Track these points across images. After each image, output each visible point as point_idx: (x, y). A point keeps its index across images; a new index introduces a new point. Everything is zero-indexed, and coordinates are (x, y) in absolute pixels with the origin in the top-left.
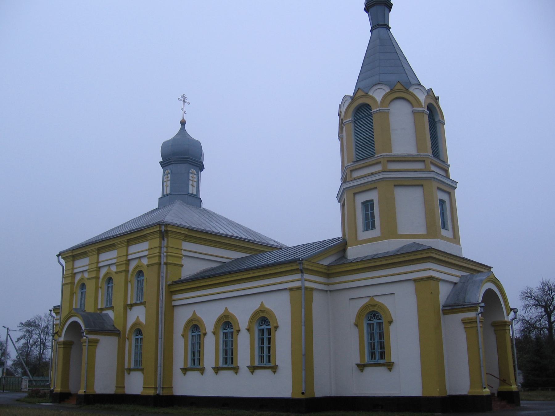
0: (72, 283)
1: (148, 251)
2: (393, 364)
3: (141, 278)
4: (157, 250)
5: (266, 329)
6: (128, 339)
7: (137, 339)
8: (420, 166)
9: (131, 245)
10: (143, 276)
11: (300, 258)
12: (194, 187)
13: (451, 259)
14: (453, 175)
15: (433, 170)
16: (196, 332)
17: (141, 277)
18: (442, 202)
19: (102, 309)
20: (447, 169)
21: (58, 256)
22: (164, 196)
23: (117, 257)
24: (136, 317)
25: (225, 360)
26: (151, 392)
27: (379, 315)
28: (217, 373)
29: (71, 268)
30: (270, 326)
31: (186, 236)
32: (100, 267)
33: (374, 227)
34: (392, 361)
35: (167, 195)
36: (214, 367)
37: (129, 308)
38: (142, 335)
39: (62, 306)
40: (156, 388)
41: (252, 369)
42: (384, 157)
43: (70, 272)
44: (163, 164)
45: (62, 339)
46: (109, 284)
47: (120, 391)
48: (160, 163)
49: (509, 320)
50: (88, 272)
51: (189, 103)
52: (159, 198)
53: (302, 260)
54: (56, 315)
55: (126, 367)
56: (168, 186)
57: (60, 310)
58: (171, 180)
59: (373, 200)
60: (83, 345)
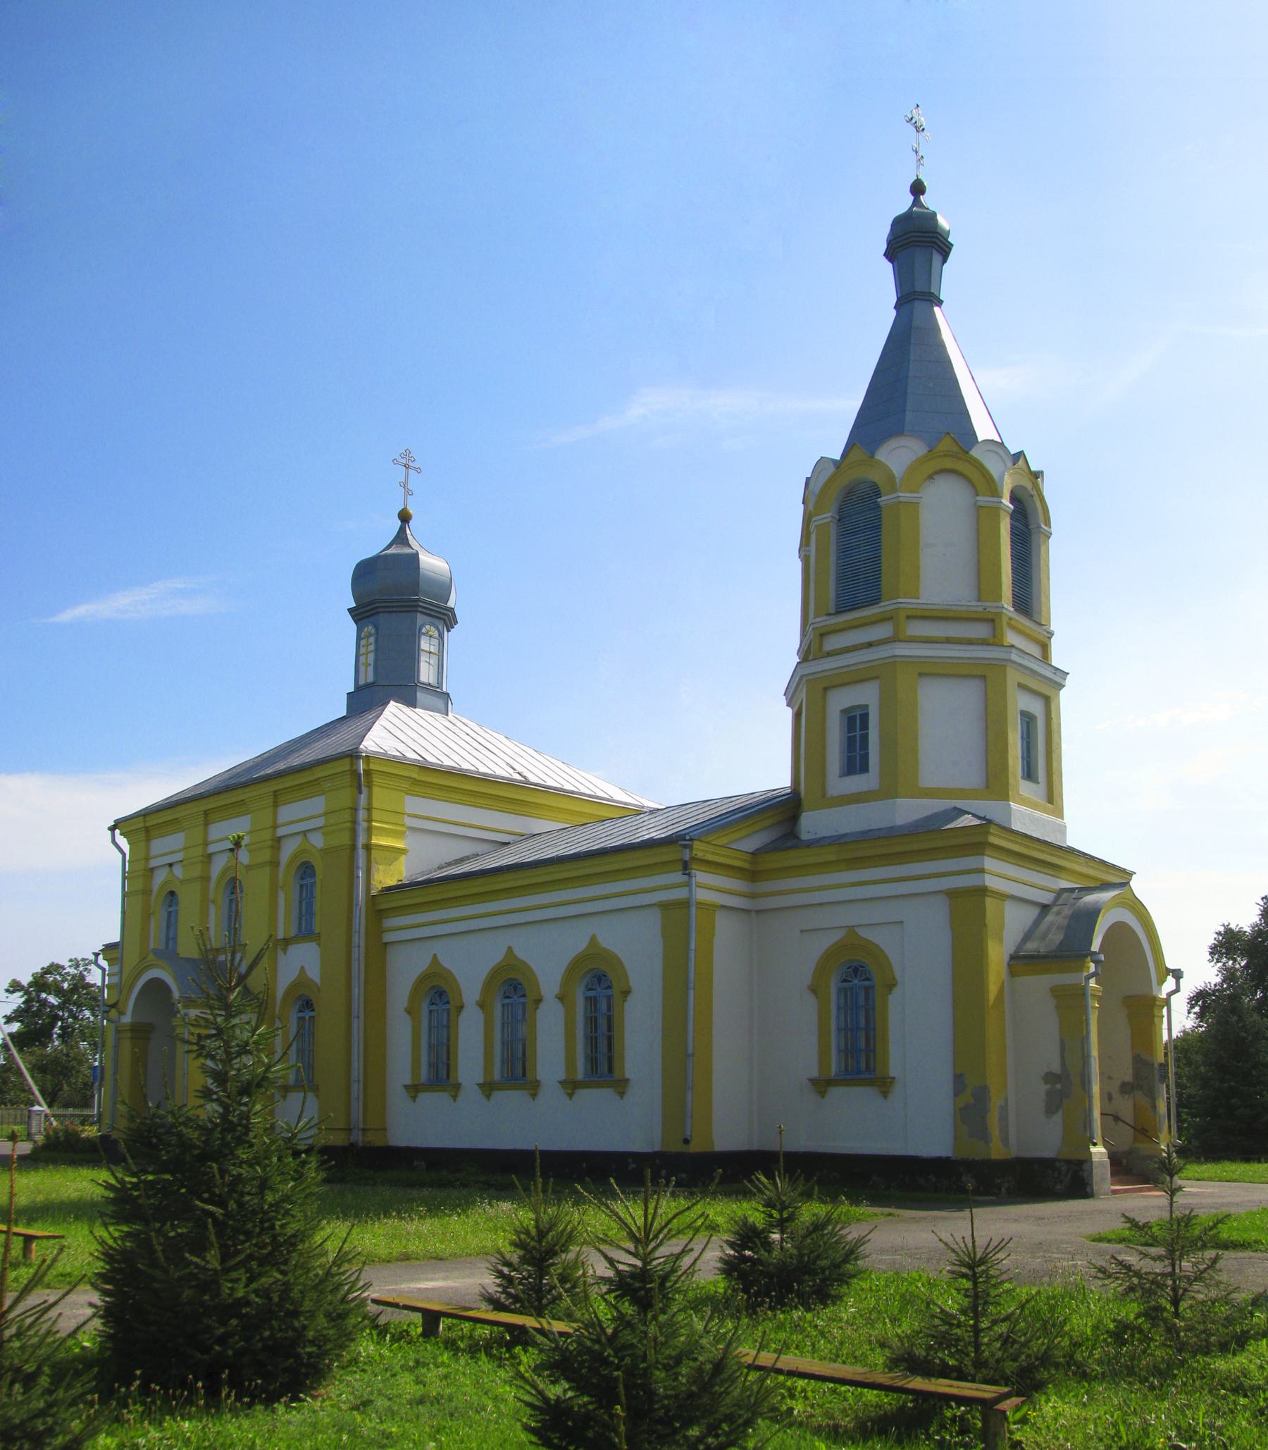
0: (147, 892)
2: (891, 1082)
3: (308, 881)
4: (347, 816)
6: (279, 1018)
7: (301, 1019)
8: (980, 631)
10: (313, 875)
11: (686, 834)
14: (1056, 661)
15: (1013, 643)
18: (1028, 719)
20: (1046, 640)
21: (112, 829)
22: (358, 688)
23: (251, 832)
28: (488, 1097)
31: (415, 782)
33: (864, 768)
34: (892, 1075)
36: (482, 1081)
37: (282, 949)
38: (313, 1010)
39: (123, 944)
40: (349, 1130)
41: (571, 1086)
42: (899, 608)
44: (358, 614)
45: (127, 1019)
48: (350, 610)
49: (1164, 996)
50: (183, 866)
51: (418, 470)
53: (691, 840)
57: (120, 950)
58: (376, 650)
59: (867, 706)
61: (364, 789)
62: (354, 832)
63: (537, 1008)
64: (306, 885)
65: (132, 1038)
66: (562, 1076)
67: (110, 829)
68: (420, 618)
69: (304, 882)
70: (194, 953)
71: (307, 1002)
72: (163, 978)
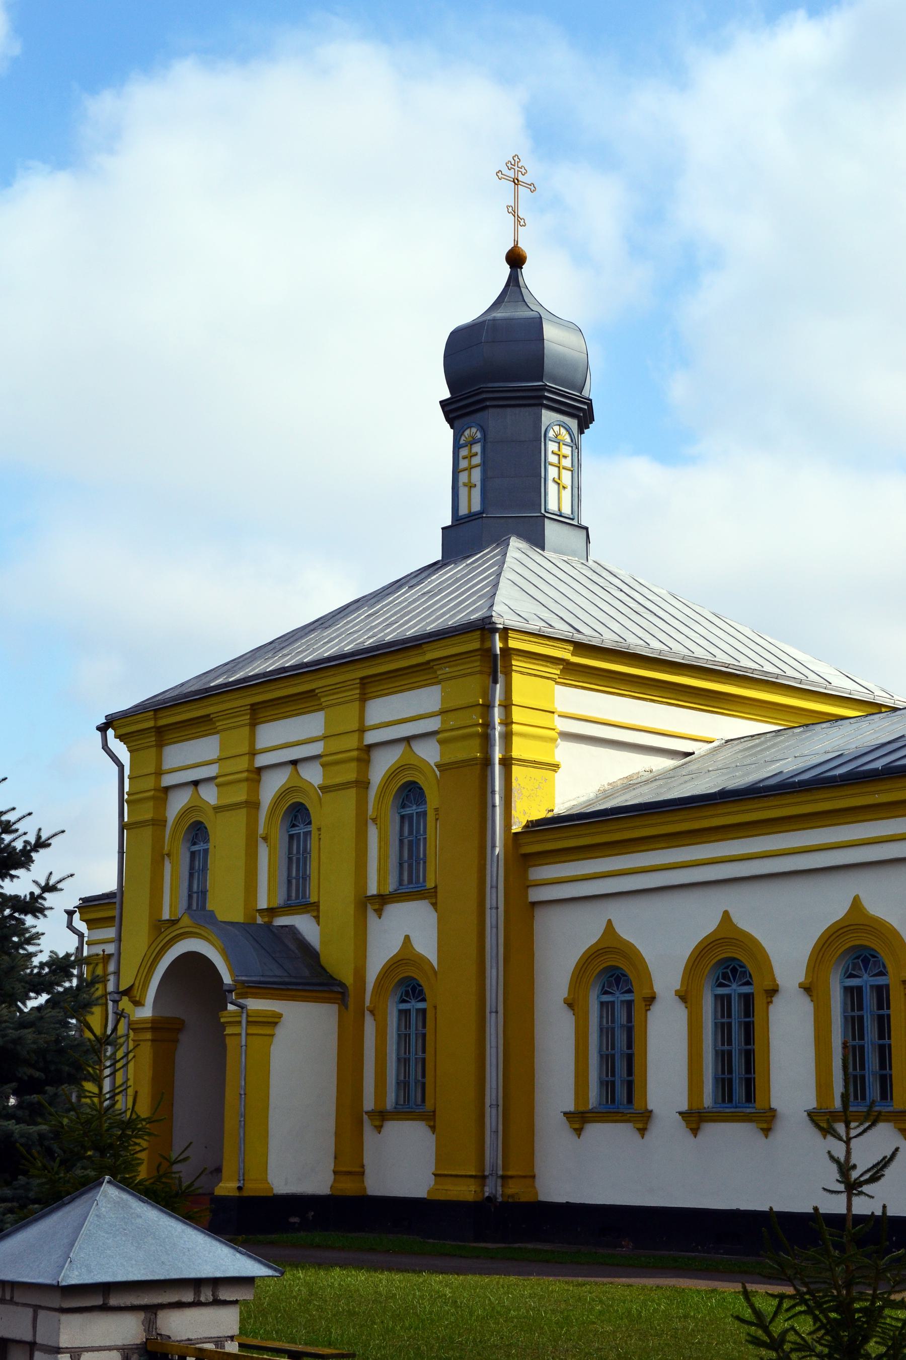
0: (159, 823)
1: (439, 718)
5: (417, 1009)
6: (372, 1012)
7: (404, 1014)
9: (371, 698)
12: (564, 488)
13: (179, 713)
16: (618, 994)
17: (414, 807)
19: (272, 912)
21: (103, 729)
24: (402, 938)
25: (724, 1086)
26: (465, 1192)
27: (745, 972)
28: (695, 1131)
29: (153, 771)
30: (751, 987)
32: (260, 770)
35: (472, 517)
37: (375, 910)
38: (424, 1000)
43: (150, 783)
45: (146, 1012)
46: (294, 826)
47: (348, 1187)
48: (444, 404)
50: (218, 786)
52: (443, 529)
54: (89, 929)
55: (369, 1104)
56: (465, 485)
58: (484, 464)
60: (229, 1030)
61: (501, 677)
62: (486, 739)
63: (770, 1002)
64: (410, 817)
65: (152, 1041)
66: (812, 1104)
67: (99, 728)
68: (548, 417)
69: (294, 831)
70: (238, 916)
71: (414, 989)
72: (190, 950)
